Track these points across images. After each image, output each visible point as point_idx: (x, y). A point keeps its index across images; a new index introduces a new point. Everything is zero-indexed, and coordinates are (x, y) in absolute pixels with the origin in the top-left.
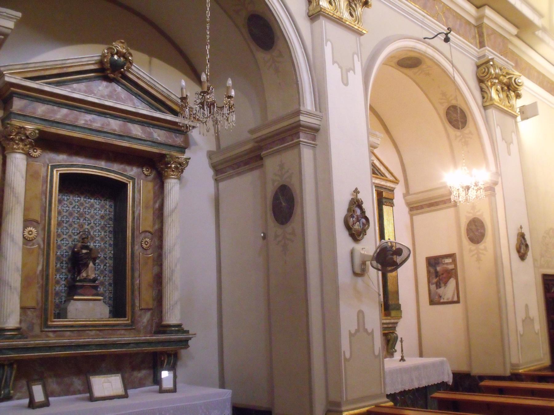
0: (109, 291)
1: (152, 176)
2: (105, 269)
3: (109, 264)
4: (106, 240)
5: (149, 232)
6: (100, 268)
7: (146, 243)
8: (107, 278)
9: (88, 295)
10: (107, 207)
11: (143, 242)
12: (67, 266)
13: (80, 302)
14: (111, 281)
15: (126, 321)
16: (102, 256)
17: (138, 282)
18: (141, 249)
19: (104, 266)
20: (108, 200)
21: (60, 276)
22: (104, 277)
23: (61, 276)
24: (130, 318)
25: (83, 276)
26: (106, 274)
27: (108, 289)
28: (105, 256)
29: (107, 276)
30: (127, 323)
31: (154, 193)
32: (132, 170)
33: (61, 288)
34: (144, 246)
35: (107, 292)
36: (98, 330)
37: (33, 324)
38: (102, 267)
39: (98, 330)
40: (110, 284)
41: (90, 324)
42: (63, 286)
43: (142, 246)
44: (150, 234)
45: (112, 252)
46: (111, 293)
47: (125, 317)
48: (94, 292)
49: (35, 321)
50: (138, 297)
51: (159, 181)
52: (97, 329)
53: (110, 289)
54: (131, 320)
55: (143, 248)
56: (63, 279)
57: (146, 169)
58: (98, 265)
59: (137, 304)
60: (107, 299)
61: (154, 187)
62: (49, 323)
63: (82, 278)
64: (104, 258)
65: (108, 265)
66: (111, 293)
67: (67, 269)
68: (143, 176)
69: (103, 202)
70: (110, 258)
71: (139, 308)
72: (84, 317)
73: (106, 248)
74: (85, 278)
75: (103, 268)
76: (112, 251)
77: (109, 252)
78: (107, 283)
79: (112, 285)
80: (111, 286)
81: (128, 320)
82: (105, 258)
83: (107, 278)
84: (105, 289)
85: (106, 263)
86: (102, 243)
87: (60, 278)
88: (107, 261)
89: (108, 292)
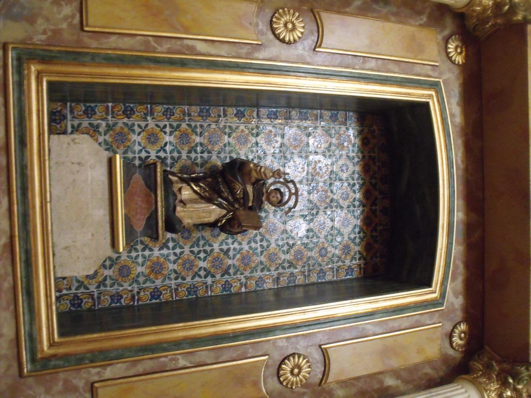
0: (138, 293)
1: (451, 352)
2: (196, 274)
3: (211, 286)
4: (272, 269)
5: (325, 373)
6: (200, 258)
7: (296, 371)
8: (173, 283)
9: (127, 204)
10: (348, 262)
11: (299, 358)
12: (197, 164)
13: (104, 178)
14: (166, 296)
15: (49, 339)
16: (230, 262)
17: (182, 362)
18: (277, 357)
19: (205, 269)
20: (362, 262)
21: (171, 143)
22: (175, 271)
23: (168, 148)
24: (61, 350)
25: (180, 190)
26: (184, 279)
27: (144, 289)
28: (231, 271)
29: (180, 280)
30: (41, 342)
31: (416, 368)
32: (456, 295)
33: (137, 148)
34: (287, 367)
35: (135, 285)
36: (12, 237)
37: (31, 20)
38: (202, 264)
39: (12, 237)
40: (156, 293)
41: (34, 207)
42: (144, 155)
43: (287, 358)
44: (320, 376)
45: (243, 290)
46: (133, 297)
47: (62, 334)
48: (140, 225)
49: (41, 24)
50: (131, 372)
51: (441, 373)
52: (17, 233)
53: (142, 294)
54: (54, 356)
55: (283, 362)
56: (162, 154)
57: (464, 332)
58: (205, 251)
59: (108, 373)
60: (113, 290)
61: (429, 362)
62: (33, 68)
63: (175, 188)
64: (225, 267)
65: (209, 280)
66: (133, 297)
67: (189, 162)
68: (449, 327)
69: (357, 248)
70: (227, 286)
71: (96, 378)
72: (55, 192)
73: (252, 272)
74: (175, 195)
75: (200, 269)
76: (246, 288)
77: (243, 280)
78: (158, 282)
79: (154, 301)
80: (153, 297)
81: (52, 344)
82: (226, 272)
83: (173, 283)
84: (141, 279)
85: (213, 276)
86: (263, 259)
87: (166, 144)
88: (218, 277)
89: (136, 290)
